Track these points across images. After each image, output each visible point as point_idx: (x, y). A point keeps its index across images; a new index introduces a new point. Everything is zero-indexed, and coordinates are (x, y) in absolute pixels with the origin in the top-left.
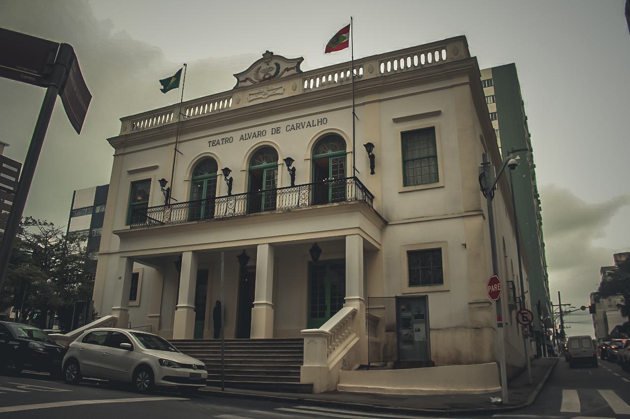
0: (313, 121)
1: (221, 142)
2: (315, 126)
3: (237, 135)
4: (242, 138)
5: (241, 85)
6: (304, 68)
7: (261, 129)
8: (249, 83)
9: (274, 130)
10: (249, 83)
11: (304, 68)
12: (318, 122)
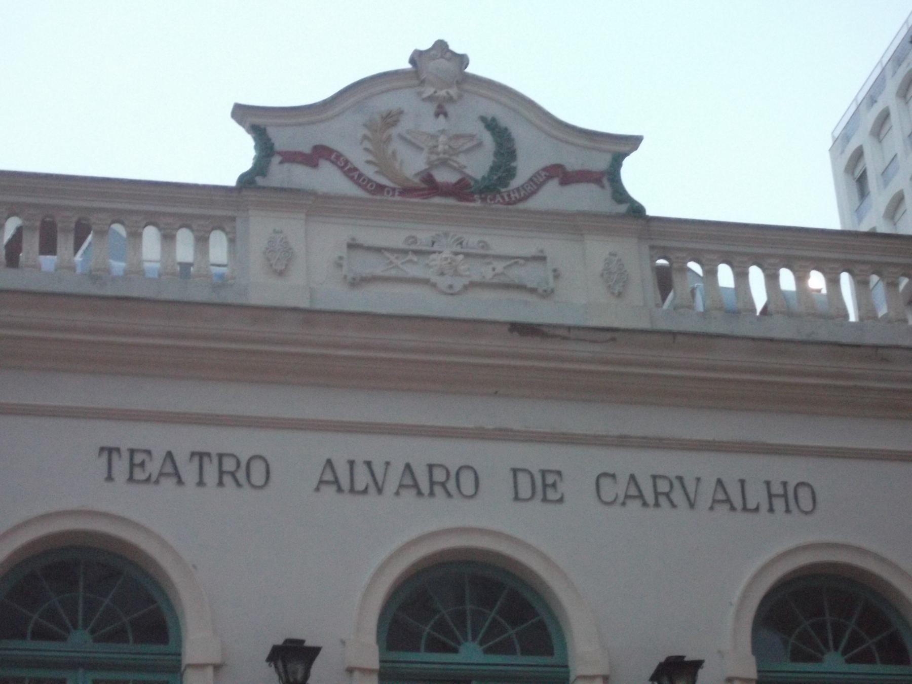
0: (742, 482)
1: (189, 472)
2: (365, 491)
3: (296, 458)
4: (330, 478)
5: (281, 174)
6: (376, 169)
7: (451, 454)
8: (327, 179)
9: (523, 479)
10: (327, 179)
11: (376, 169)
12: (770, 496)
